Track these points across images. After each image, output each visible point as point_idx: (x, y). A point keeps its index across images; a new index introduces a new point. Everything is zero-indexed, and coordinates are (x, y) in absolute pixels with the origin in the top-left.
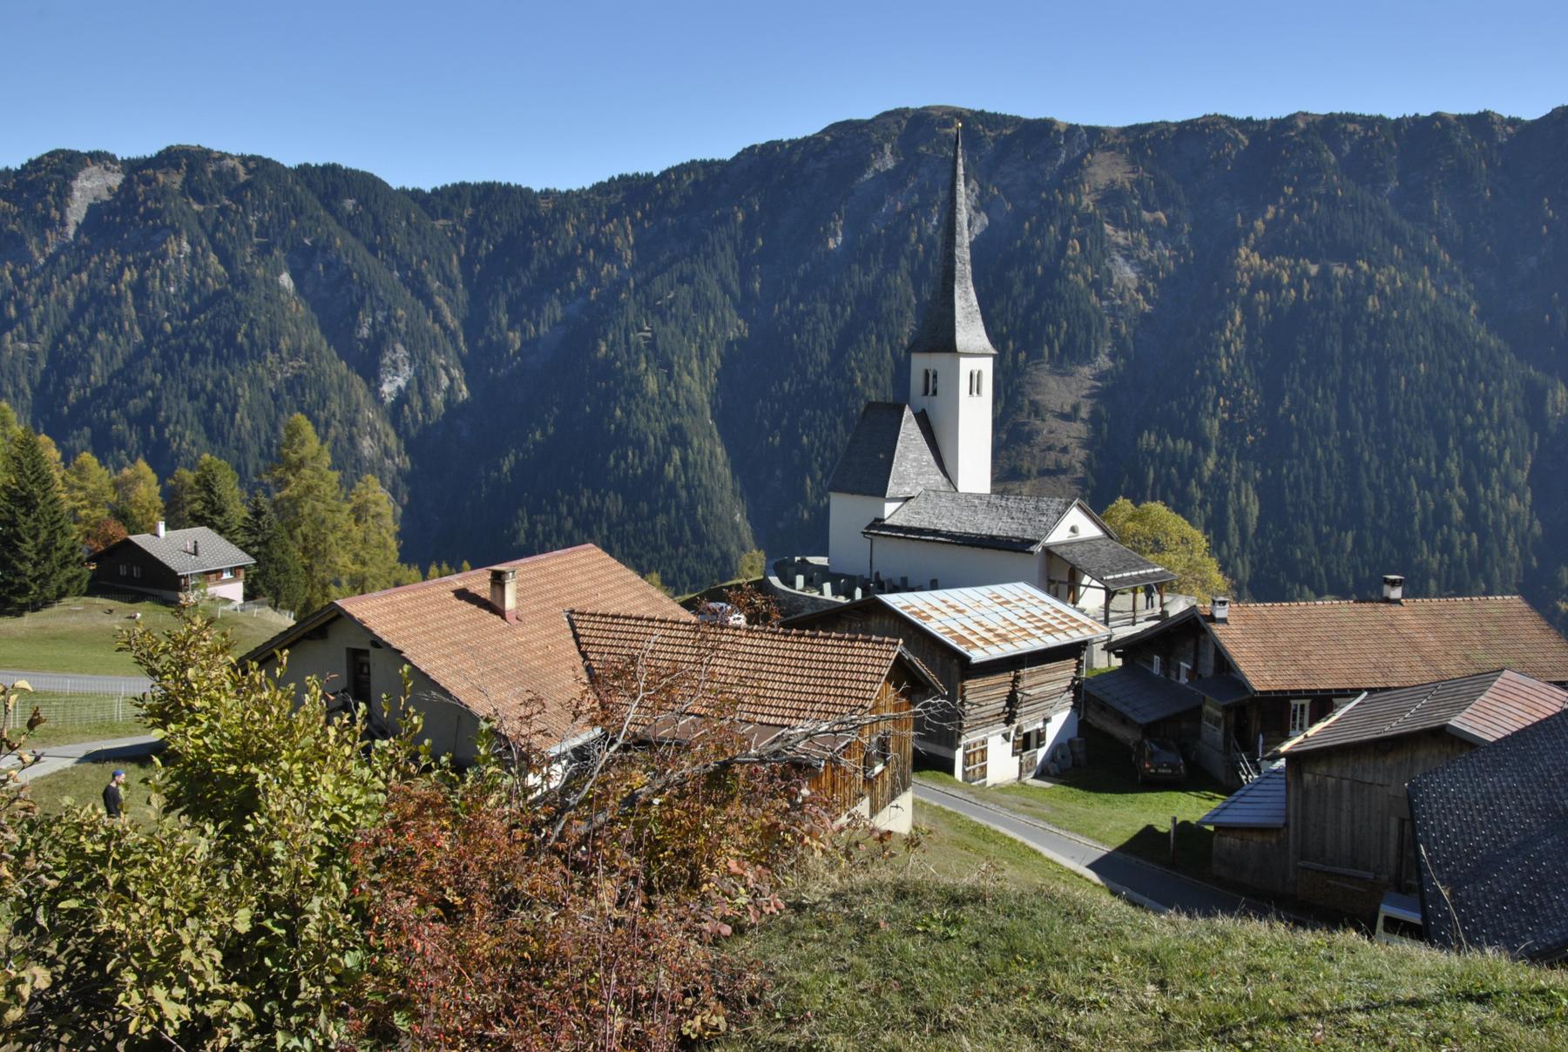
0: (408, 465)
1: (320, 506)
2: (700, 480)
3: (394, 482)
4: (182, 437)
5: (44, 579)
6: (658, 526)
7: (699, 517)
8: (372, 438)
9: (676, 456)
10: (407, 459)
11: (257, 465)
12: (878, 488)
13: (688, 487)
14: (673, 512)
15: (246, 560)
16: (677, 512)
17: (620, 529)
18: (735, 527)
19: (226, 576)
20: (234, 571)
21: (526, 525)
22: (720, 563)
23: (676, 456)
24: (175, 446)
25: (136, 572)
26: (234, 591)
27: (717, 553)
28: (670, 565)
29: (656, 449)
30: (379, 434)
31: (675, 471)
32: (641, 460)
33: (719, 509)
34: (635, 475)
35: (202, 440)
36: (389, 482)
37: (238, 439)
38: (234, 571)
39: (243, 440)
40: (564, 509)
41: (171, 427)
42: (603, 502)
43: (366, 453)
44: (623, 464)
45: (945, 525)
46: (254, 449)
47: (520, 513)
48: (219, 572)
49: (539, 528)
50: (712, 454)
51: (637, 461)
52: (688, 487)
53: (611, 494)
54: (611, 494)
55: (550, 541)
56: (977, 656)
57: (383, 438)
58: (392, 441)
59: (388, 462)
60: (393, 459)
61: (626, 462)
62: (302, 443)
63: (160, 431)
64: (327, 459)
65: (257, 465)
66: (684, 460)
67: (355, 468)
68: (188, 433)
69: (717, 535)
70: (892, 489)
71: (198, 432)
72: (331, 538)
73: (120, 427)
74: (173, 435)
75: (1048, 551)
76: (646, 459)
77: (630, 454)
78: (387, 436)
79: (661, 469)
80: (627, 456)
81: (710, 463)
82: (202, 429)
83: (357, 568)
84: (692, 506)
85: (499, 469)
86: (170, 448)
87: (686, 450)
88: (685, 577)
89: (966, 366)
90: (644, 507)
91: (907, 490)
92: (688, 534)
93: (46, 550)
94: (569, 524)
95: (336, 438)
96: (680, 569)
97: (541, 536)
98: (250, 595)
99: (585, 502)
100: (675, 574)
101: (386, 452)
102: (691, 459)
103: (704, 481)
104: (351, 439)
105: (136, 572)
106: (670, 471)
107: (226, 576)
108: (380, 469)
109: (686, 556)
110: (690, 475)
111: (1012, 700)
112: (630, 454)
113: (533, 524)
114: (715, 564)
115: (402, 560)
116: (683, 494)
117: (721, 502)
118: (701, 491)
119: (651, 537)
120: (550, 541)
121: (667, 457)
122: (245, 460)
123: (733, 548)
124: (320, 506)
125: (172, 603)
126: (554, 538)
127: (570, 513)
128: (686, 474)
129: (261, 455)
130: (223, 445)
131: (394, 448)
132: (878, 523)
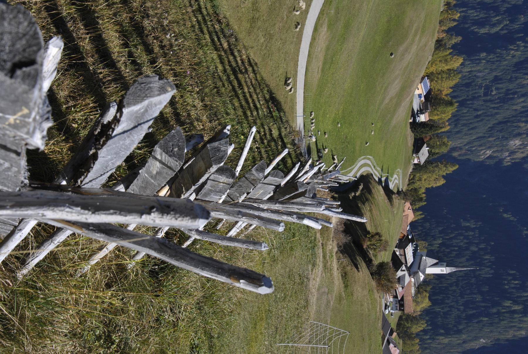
0: (506, 164)
1: (437, 172)
2: (503, 320)
3: (495, 157)
4: (517, 50)
5: (417, 132)
6: (475, 296)
7: (481, 319)
8: (521, 145)
9: (516, 308)
10: (509, 163)
11: (502, 88)
12: (427, 256)
13: (498, 313)
14: (483, 304)
15: (422, 163)
16: (484, 307)
17: (472, 275)
18: (476, 338)
19: (419, 160)
20: (420, 162)
21: (473, 226)
22: (455, 329)
23: (516, 308)
24: (512, 47)
25: (419, 145)
26: (416, 161)
27: (461, 327)
28: (453, 301)
29: (521, 297)
30: (523, 148)
31: (508, 307)
32: (513, 288)
33: (487, 330)
34: (505, 284)
35: (515, 60)
36: (495, 155)
37: (516, 78)
38: (420, 162)
39: (516, 80)
40: (482, 246)
41: (522, 44)
42: (488, 267)
43: (512, 142)
44: (510, 278)
45: (422, 263)
46: (511, 86)
47: (480, 223)
48: (419, 159)
49: (471, 233)
50: (520, 329)
51: (513, 286)
52: (498, 313)
53: (493, 271)
54: (493, 271)
55: (464, 239)
56: (406, 249)
57: (521, 151)
58: (519, 155)
59: (507, 154)
60: (508, 156)
61: (511, 280)
62: (451, 167)
63: (520, 39)
64: (448, 172)
65: (502, 88)
66: (515, 312)
67: (502, 138)
68: (519, 53)
69: (471, 328)
70: (427, 258)
71: (520, 58)
72: (430, 174)
73: (522, 19)
74: (518, 46)
75: (418, 272)
76: (514, 290)
77: (517, 282)
78: (522, 153)
79: (509, 299)
80: (515, 280)
81: (515, 326)
82: (521, 59)
83: (423, 179)
84: (488, 315)
85: (505, 212)
86: (511, 46)
87: (521, 313)
88: (446, 310)
89: (444, 269)
90: (486, 289)
91: (427, 260)
92: (471, 312)
93: (422, 132)
94: (474, 248)
95: (520, 127)
96: (451, 307)
97: (467, 234)
98: (415, 164)
99: (487, 257)
100: (448, 304)
101: (512, 153)
102: (516, 316)
103: (502, 322)
104: (519, 134)
105: (419, 145)
106: (508, 303)
107: (419, 160)
108: (502, 150)
109: (459, 310)
110: (506, 315)
111: (402, 255)
112: (517, 282)
113: (473, 230)
114: (455, 326)
115: (426, 188)
116: (494, 310)
117: (491, 332)
118: (497, 320)
119: (468, 291)
120: (464, 239)
121: (516, 302)
122: (505, 82)
123: (464, 336)
124: (437, 172)
125: (413, 153)
126: (465, 241)
127: (480, 249)
128: (507, 312)
129: (508, 90)
130: (513, 71)
131: (515, 157)
132: (422, 256)
